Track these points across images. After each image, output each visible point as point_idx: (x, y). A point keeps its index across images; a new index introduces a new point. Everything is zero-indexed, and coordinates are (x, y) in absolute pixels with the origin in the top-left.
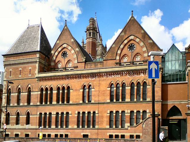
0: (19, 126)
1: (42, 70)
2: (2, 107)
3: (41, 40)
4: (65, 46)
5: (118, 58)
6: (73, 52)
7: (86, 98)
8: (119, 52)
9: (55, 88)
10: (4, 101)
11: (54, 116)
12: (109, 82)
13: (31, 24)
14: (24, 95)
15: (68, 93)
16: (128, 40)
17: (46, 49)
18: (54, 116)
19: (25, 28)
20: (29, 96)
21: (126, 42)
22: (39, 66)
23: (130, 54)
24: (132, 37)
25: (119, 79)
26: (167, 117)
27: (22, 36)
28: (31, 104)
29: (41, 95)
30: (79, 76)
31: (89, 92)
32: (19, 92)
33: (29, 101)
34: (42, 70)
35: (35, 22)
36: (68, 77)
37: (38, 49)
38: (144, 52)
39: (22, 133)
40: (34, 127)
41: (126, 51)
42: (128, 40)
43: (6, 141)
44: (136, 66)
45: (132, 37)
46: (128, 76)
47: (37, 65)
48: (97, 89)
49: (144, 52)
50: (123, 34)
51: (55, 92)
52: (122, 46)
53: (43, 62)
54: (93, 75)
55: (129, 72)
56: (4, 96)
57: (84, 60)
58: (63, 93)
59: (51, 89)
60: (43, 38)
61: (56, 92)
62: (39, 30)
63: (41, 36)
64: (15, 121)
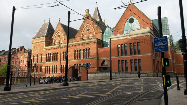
0: (38, 73)
1: (47, 45)
3: (48, 30)
4: (59, 31)
6: (62, 34)
9: (82, 50)
11: (51, 67)
14: (40, 57)
16: (86, 26)
18: (51, 67)
24: (88, 25)
25: (78, 48)
26: (101, 66)
29: (46, 57)
31: (89, 52)
32: (38, 56)
34: (47, 45)
36: (88, 43)
37: (45, 35)
38: (93, 32)
39: (38, 76)
40: (43, 73)
42: (86, 26)
43: (83, 80)
44: (155, 26)
45: (88, 25)
46: (81, 46)
47: (45, 42)
49: (93, 32)
50: (84, 23)
51: (82, 52)
55: (82, 44)
60: (49, 29)
64: (40, 71)
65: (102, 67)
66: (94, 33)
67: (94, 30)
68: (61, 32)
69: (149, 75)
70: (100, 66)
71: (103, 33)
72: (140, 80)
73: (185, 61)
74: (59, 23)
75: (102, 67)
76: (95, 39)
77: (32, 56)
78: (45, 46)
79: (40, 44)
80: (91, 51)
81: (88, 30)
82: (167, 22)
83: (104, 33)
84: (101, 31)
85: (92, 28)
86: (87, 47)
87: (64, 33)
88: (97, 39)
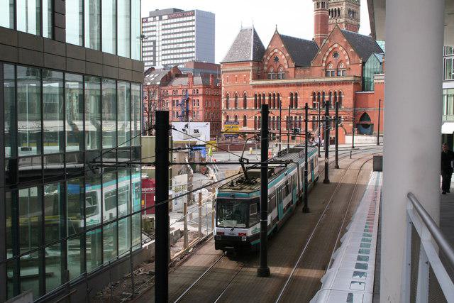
2: (65, 183)
4: (276, 51)
5: (324, 65)
6: (283, 57)
7: (293, 103)
8: (325, 59)
10: (223, 105)
12: (312, 91)
13: (245, 26)
14: (241, 99)
15: (296, 99)
17: (260, 51)
19: (237, 32)
20: (245, 101)
21: (331, 49)
22: (253, 74)
23: (334, 61)
25: (320, 89)
27: (236, 41)
28: (247, 108)
29: (256, 100)
30: (288, 85)
33: (245, 106)
35: (247, 25)
41: (331, 58)
45: (336, 46)
48: (302, 96)
52: (327, 54)
53: (256, 68)
54: (298, 85)
56: (223, 100)
57: (294, 66)
58: (260, 100)
59: (264, 95)
61: (328, 97)
62: (250, 54)
63: (254, 39)
65: (361, 123)
66: (348, 63)
67: (347, 57)
68: (280, 53)
69: (96, 41)
70: (358, 122)
71: (364, 64)
72: (378, 149)
73: (311, 273)
74: (277, 34)
75: (361, 123)
76: (349, 76)
77: (223, 96)
78: (253, 79)
79: (240, 75)
80: (343, 96)
81: (336, 55)
82: (441, 200)
83: (366, 65)
84: (361, 61)
85: (344, 52)
86: (337, 88)
87: (287, 55)
88: (354, 76)
